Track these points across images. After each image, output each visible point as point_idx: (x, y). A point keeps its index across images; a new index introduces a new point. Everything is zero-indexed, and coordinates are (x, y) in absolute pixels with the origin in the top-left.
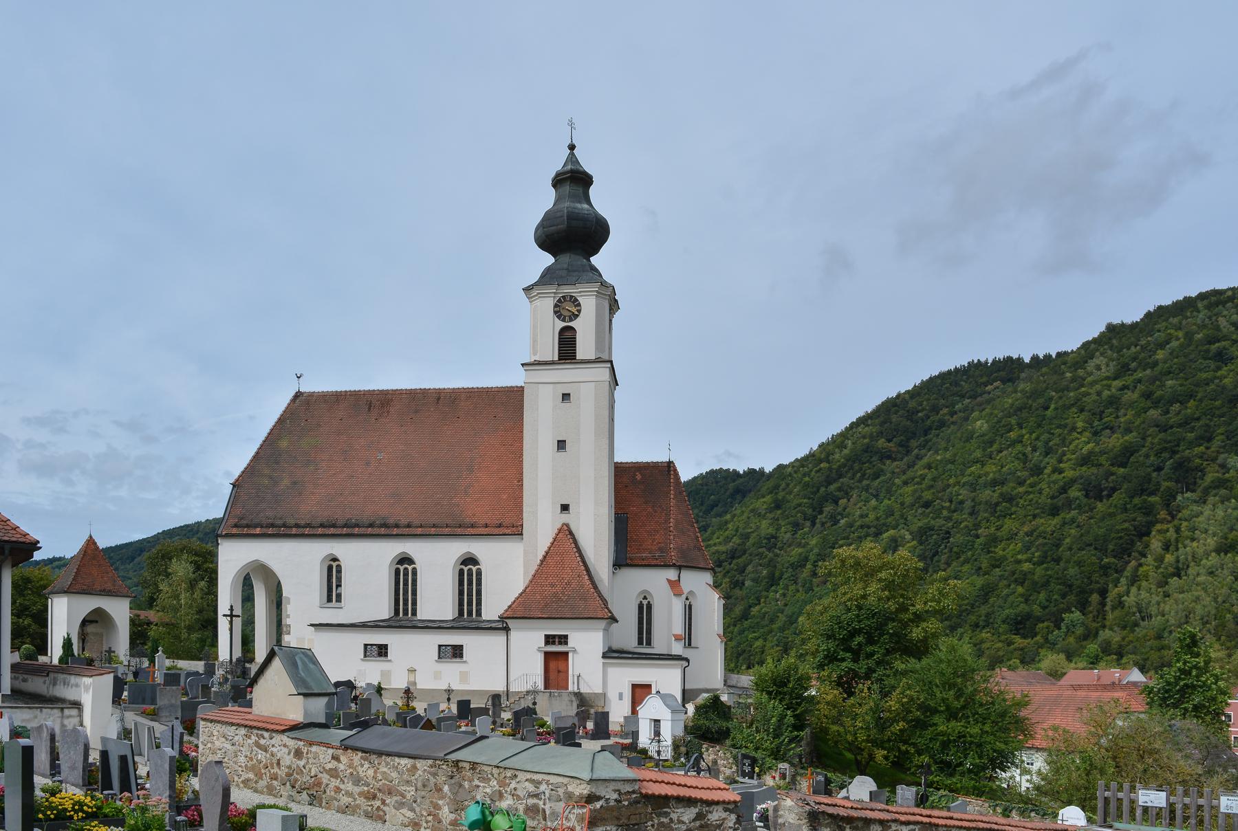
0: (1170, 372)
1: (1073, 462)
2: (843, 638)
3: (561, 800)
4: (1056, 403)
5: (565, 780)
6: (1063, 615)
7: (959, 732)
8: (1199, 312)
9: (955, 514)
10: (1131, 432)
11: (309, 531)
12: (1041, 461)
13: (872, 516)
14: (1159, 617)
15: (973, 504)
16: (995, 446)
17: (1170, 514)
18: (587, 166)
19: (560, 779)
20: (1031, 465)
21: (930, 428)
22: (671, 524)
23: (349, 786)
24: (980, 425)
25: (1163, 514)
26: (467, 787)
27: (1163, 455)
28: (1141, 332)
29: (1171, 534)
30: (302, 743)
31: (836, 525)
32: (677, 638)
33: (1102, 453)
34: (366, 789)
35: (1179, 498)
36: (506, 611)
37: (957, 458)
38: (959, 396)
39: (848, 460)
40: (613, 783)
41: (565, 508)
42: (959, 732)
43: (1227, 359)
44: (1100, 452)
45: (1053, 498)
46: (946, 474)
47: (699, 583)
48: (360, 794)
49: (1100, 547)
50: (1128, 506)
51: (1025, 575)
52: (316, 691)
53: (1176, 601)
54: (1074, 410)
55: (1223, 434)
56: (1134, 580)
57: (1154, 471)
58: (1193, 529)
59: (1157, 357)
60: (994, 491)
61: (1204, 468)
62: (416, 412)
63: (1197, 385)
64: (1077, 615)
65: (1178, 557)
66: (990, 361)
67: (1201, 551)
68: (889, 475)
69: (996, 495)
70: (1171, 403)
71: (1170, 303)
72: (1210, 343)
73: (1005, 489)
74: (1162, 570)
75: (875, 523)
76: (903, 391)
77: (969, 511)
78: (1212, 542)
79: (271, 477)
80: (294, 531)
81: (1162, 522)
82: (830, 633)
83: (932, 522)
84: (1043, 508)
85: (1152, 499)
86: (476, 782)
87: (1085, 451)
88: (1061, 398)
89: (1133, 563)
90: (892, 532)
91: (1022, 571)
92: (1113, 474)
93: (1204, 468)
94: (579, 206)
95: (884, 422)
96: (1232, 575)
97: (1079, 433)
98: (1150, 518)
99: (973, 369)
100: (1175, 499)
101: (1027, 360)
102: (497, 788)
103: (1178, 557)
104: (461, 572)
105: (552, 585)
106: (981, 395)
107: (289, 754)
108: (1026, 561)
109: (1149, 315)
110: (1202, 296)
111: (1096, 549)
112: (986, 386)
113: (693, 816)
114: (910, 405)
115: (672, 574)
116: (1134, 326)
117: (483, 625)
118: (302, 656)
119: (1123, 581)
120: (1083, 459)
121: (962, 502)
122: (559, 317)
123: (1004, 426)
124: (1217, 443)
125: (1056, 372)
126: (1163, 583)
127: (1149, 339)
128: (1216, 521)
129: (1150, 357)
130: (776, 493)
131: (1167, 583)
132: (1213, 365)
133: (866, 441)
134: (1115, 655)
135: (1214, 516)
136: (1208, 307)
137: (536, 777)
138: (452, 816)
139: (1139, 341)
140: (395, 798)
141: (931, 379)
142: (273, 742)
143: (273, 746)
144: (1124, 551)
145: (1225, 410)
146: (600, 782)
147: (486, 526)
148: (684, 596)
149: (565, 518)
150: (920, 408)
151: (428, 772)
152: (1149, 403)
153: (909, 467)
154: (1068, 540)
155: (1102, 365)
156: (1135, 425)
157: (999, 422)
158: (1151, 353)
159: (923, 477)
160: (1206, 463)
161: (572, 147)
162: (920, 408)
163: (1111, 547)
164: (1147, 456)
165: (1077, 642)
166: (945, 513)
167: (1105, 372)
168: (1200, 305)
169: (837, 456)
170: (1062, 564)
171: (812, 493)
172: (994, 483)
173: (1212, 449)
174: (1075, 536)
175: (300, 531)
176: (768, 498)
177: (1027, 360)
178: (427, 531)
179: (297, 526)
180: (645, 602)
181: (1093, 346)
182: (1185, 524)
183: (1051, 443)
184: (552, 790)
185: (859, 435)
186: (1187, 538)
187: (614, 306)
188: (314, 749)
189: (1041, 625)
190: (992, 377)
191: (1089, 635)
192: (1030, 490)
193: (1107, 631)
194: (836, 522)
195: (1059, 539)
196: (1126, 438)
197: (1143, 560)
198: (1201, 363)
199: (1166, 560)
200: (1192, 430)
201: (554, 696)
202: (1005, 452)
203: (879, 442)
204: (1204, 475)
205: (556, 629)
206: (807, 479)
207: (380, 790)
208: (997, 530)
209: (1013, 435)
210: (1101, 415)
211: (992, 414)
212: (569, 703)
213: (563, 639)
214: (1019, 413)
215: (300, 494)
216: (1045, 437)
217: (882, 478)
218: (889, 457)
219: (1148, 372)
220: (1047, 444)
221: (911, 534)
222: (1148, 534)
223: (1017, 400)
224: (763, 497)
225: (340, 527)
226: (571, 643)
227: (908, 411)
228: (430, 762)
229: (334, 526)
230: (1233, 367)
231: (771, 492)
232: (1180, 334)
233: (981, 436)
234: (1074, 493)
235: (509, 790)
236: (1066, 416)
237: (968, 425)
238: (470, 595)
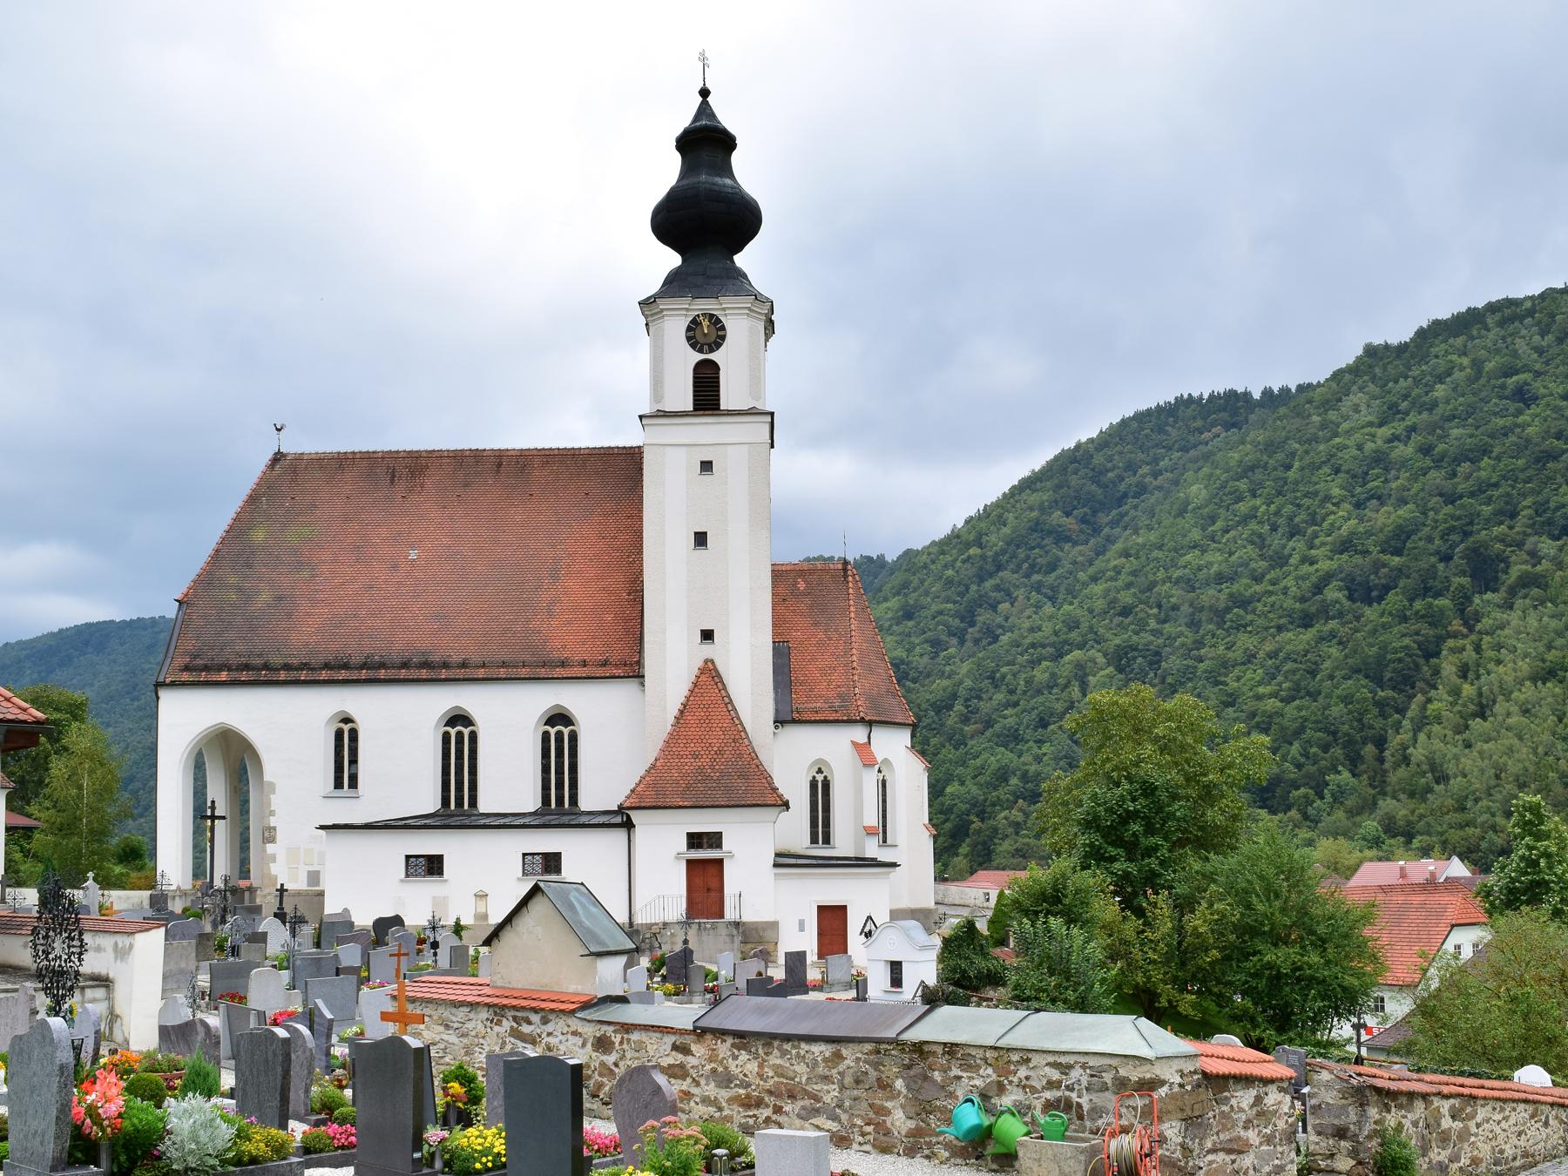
0: (1454, 417)
1: (1328, 547)
2: (1111, 825)
3: (1107, 1089)
4: (1301, 460)
5: (1114, 1062)
6: (1327, 777)
7: (1294, 963)
8: (1488, 330)
9: (1167, 625)
10: (1406, 503)
11: (307, 675)
12: (1284, 547)
13: (1048, 628)
14: (1459, 779)
15: (1191, 610)
16: (1219, 524)
17: (1466, 624)
18: (727, 118)
19: (1108, 1061)
20: (1271, 553)
21: (1125, 495)
22: (855, 658)
23: (711, 1090)
24: (1196, 491)
25: (1456, 625)
26: (939, 1079)
27: (1451, 537)
28: (1413, 357)
29: (1470, 655)
30: (611, 1028)
31: (995, 642)
32: (870, 832)
33: (1369, 534)
34: (742, 1091)
35: (1477, 600)
36: (628, 797)
37: (1166, 541)
38: (1164, 447)
39: (1008, 544)
40: (1176, 1061)
41: (707, 635)
42: (1294, 963)
43: (1530, 399)
44: (1366, 533)
45: (1303, 600)
46: (1151, 566)
47: (894, 746)
48: (730, 1100)
49: (1373, 672)
50: (1408, 613)
51: (1270, 717)
52: (612, 949)
53: (1481, 753)
54: (1327, 470)
55: (1530, 507)
56: (1420, 724)
57: (1441, 560)
58: (1499, 647)
59: (1436, 394)
60: (1220, 591)
61: (1508, 557)
62: (466, 485)
63: (1492, 436)
64: (1346, 775)
65: (1480, 688)
66: (1206, 396)
67: (1509, 679)
68: (1068, 566)
69: (1223, 597)
70: (1458, 460)
71: (1449, 316)
72: (1507, 375)
73: (1235, 587)
74: (1458, 708)
75: (1054, 638)
76: (1084, 440)
77: (1186, 620)
78: (1524, 666)
79: (240, 589)
80: (283, 675)
81: (1455, 636)
82: (1090, 818)
83: (1135, 638)
84: (1290, 616)
85: (1443, 602)
86: (955, 1072)
87: (1344, 531)
88: (1307, 452)
89: (1420, 698)
90: (1077, 654)
91: (1266, 711)
92: (1384, 565)
93: (1508, 557)
94: (718, 180)
95: (1058, 487)
96: (1553, 714)
97: (1336, 505)
98: (1440, 631)
99: (1182, 408)
100: (1471, 602)
101: (1257, 395)
102: (994, 1077)
103: (1480, 688)
104: (546, 737)
105: (696, 756)
106: (1195, 446)
107: (584, 1045)
108: (1271, 696)
109: (1421, 334)
110: (1492, 308)
111: (1367, 676)
112: (1202, 433)
113: (1252, 1100)
114: (1095, 461)
115: (859, 734)
116: (1402, 348)
117: (584, 820)
118: (577, 894)
119: (1406, 723)
120: (1343, 543)
121: (1175, 608)
122: (693, 346)
123: (1230, 493)
124: (1520, 523)
125: (1298, 415)
126: (1462, 728)
127: (1424, 367)
128: (1528, 634)
129: (1427, 393)
130: (906, 595)
131: (1467, 727)
132: (1513, 407)
133: (1035, 514)
134: (1401, 836)
135: (1526, 627)
136: (1502, 324)
137: (1063, 1060)
138: (911, 1124)
139: (1410, 370)
140: (800, 1103)
141: (1124, 423)
142: (550, 1027)
143: (549, 1034)
144: (1406, 682)
145: (1531, 472)
146: (1164, 1061)
147: (584, 664)
148: (877, 767)
149: (708, 650)
150: (1110, 465)
151: (866, 1062)
152: (1428, 462)
153: (1098, 554)
154: (1327, 664)
155: (1361, 405)
156: (1412, 493)
157: (1223, 487)
158: (1428, 389)
159: (1118, 571)
160: (1509, 549)
161: (705, 93)
162: (1110, 465)
163: (1388, 675)
164: (1430, 539)
165: (1348, 819)
166: (1153, 624)
167: (1366, 416)
168: (1490, 321)
169: (993, 538)
170: (1321, 699)
171: (959, 594)
172: (1220, 578)
173: (1517, 529)
174: (1337, 658)
175: (293, 675)
176: (894, 603)
177: (1257, 395)
178: (493, 673)
179: (287, 667)
180: (820, 778)
181: (1347, 377)
182: (1487, 639)
183: (1297, 520)
184: (1092, 1076)
185: (1024, 506)
186: (1491, 659)
187: (770, 327)
188: (635, 1036)
189: (1295, 793)
190: (1209, 420)
191: (1369, 806)
192: (1271, 588)
193: (1389, 800)
194: (996, 639)
195: (1316, 663)
196: (1400, 512)
197: (1433, 693)
198: (1495, 403)
199: (1464, 693)
200: (1489, 501)
201: (705, 929)
202: (1233, 533)
203: (1053, 516)
204: (1508, 567)
205: (704, 822)
206: (950, 572)
207: (770, 1092)
208: (1227, 649)
209: (1243, 507)
210: (1364, 478)
211: (1211, 475)
212: (728, 939)
213: (714, 840)
214: (1250, 474)
215: (289, 616)
216: (1288, 509)
217: (1060, 571)
218: (1068, 539)
219: (1425, 415)
220: (1291, 520)
221: (1105, 655)
222: (1437, 654)
223: (1247, 455)
224: (886, 600)
225: (357, 669)
226: (727, 843)
227: (1093, 470)
228: (868, 1047)
229: (346, 666)
230: (1538, 410)
231: (898, 593)
232: (1465, 361)
233: (1199, 508)
234: (1333, 593)
235: (1015, 1080)
236: (1317, 480)
237: (1179, 492)
238: (560, 772)
